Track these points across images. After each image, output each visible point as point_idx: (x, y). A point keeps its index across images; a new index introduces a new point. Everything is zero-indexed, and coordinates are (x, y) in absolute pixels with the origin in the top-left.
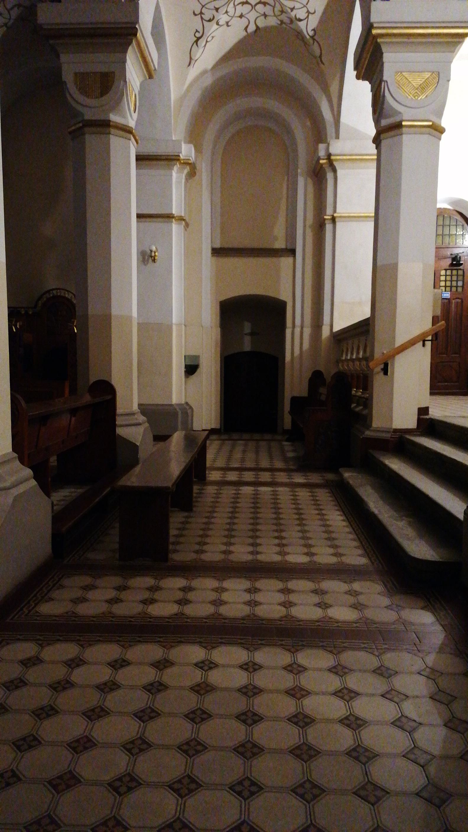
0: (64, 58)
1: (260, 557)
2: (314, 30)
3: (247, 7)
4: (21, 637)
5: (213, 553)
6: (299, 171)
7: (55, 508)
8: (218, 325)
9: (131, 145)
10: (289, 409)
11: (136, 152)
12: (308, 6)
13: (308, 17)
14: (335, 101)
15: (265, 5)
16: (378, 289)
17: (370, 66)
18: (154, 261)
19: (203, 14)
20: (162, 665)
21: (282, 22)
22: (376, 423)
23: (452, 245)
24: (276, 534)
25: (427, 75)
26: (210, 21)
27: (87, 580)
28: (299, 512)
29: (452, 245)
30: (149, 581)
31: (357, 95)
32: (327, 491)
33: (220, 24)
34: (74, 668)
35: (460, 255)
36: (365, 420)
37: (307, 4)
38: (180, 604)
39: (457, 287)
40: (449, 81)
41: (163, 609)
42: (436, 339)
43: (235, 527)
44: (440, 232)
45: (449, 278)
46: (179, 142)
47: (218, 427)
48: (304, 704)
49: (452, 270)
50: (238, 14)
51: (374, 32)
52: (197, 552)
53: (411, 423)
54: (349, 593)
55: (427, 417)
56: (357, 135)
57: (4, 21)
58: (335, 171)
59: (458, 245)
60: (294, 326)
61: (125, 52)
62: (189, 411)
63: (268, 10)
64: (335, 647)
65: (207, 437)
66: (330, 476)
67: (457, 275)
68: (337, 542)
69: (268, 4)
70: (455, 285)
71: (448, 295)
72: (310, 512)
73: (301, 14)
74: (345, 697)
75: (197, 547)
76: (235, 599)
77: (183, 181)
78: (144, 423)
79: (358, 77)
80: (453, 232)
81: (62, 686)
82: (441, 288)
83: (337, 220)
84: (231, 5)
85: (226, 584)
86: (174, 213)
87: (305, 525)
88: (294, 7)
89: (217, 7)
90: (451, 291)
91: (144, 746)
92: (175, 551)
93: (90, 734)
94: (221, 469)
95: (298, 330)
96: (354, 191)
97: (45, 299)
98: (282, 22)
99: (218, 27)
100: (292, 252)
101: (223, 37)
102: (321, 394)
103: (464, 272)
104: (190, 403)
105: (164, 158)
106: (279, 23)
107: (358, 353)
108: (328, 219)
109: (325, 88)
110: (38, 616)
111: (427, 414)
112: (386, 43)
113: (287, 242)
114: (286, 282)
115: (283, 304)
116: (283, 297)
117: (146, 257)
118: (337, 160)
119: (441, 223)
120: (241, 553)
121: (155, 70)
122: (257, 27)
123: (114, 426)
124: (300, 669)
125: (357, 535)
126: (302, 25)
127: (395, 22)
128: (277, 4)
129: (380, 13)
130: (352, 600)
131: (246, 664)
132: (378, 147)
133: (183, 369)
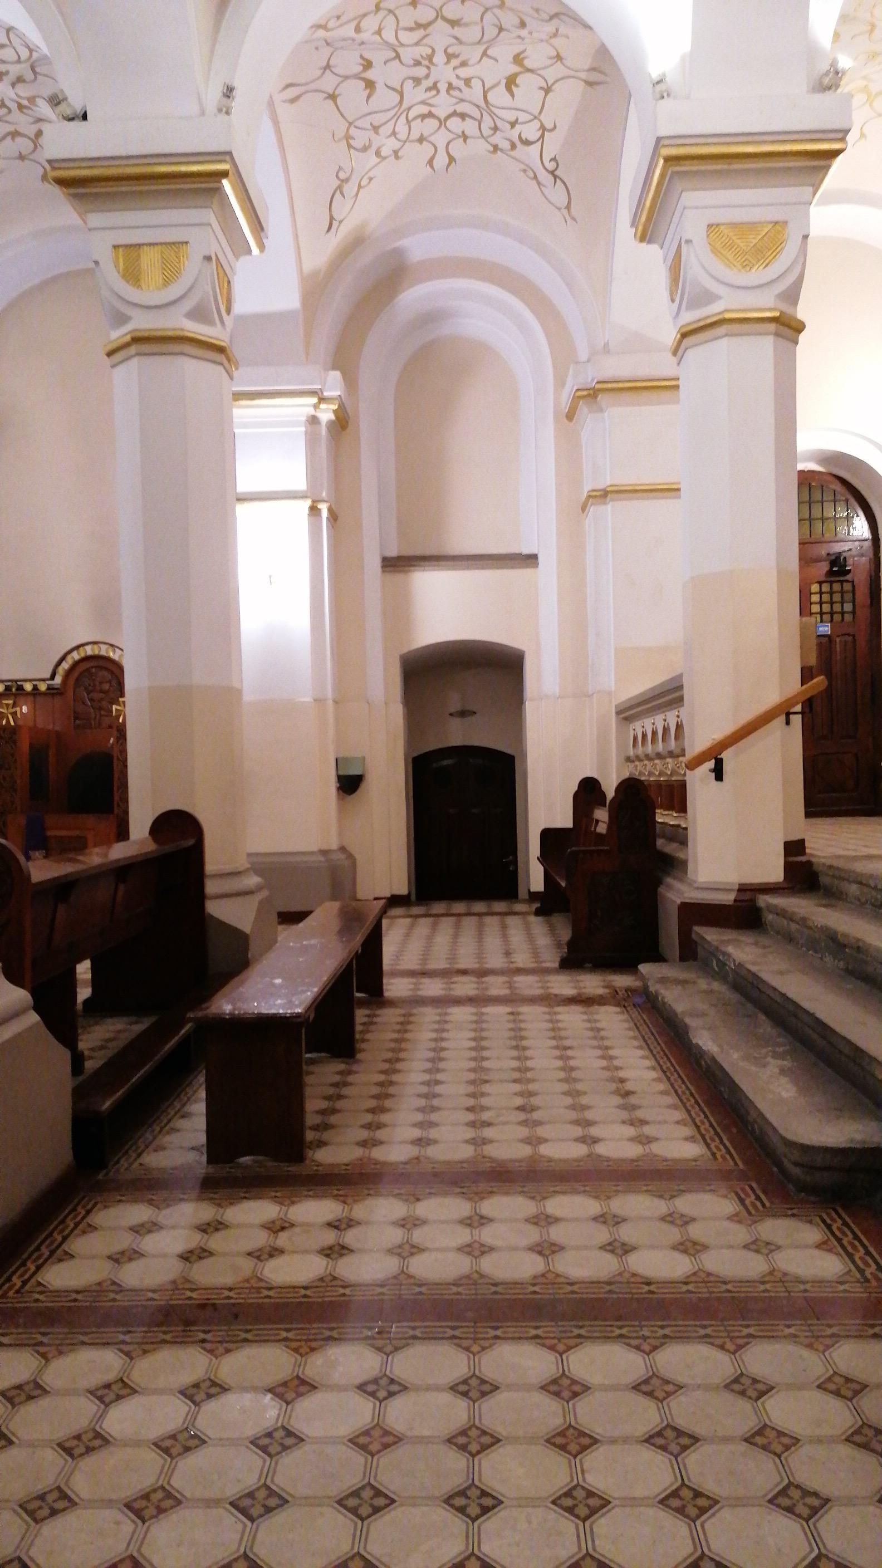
2: (554, 159)
3: (432, 124)
7: (90, 1065)
13: (542, 136)
15: (463, 119)
23: (828, 536)
26: (365, 149)
33: (383, 154)
34: (111, 1402)
35: (844, 554)
37: (540, 113)
39: (843, 613)
41: (296, 1269)
43: (438, 1089)
45: (826, 597)
49: (831, 582)
50: (415, 135)
52: (364, 1144)
55: (803, 859)
59: (840, 536)
63: (470, 127)
65: (384, 912)
66: (623, 981)
67: (842, 592)
70: (839, 609)
78: (260, 888)
80: (829, 512)
81: (84, 1444)
84: (403, 119)
87: (562, 1069)
88: (517, 119)
89: (376, 124)
90: (831, 621)
92: (321, 1144)
93: (139, 1551)
94: (412, 974)
99: (378, 160)
102: (597, 821)
103: (854, 587)
106: (492, 149)
110: (41, 1293)
123: (200, 897)
130: (674, 1234)
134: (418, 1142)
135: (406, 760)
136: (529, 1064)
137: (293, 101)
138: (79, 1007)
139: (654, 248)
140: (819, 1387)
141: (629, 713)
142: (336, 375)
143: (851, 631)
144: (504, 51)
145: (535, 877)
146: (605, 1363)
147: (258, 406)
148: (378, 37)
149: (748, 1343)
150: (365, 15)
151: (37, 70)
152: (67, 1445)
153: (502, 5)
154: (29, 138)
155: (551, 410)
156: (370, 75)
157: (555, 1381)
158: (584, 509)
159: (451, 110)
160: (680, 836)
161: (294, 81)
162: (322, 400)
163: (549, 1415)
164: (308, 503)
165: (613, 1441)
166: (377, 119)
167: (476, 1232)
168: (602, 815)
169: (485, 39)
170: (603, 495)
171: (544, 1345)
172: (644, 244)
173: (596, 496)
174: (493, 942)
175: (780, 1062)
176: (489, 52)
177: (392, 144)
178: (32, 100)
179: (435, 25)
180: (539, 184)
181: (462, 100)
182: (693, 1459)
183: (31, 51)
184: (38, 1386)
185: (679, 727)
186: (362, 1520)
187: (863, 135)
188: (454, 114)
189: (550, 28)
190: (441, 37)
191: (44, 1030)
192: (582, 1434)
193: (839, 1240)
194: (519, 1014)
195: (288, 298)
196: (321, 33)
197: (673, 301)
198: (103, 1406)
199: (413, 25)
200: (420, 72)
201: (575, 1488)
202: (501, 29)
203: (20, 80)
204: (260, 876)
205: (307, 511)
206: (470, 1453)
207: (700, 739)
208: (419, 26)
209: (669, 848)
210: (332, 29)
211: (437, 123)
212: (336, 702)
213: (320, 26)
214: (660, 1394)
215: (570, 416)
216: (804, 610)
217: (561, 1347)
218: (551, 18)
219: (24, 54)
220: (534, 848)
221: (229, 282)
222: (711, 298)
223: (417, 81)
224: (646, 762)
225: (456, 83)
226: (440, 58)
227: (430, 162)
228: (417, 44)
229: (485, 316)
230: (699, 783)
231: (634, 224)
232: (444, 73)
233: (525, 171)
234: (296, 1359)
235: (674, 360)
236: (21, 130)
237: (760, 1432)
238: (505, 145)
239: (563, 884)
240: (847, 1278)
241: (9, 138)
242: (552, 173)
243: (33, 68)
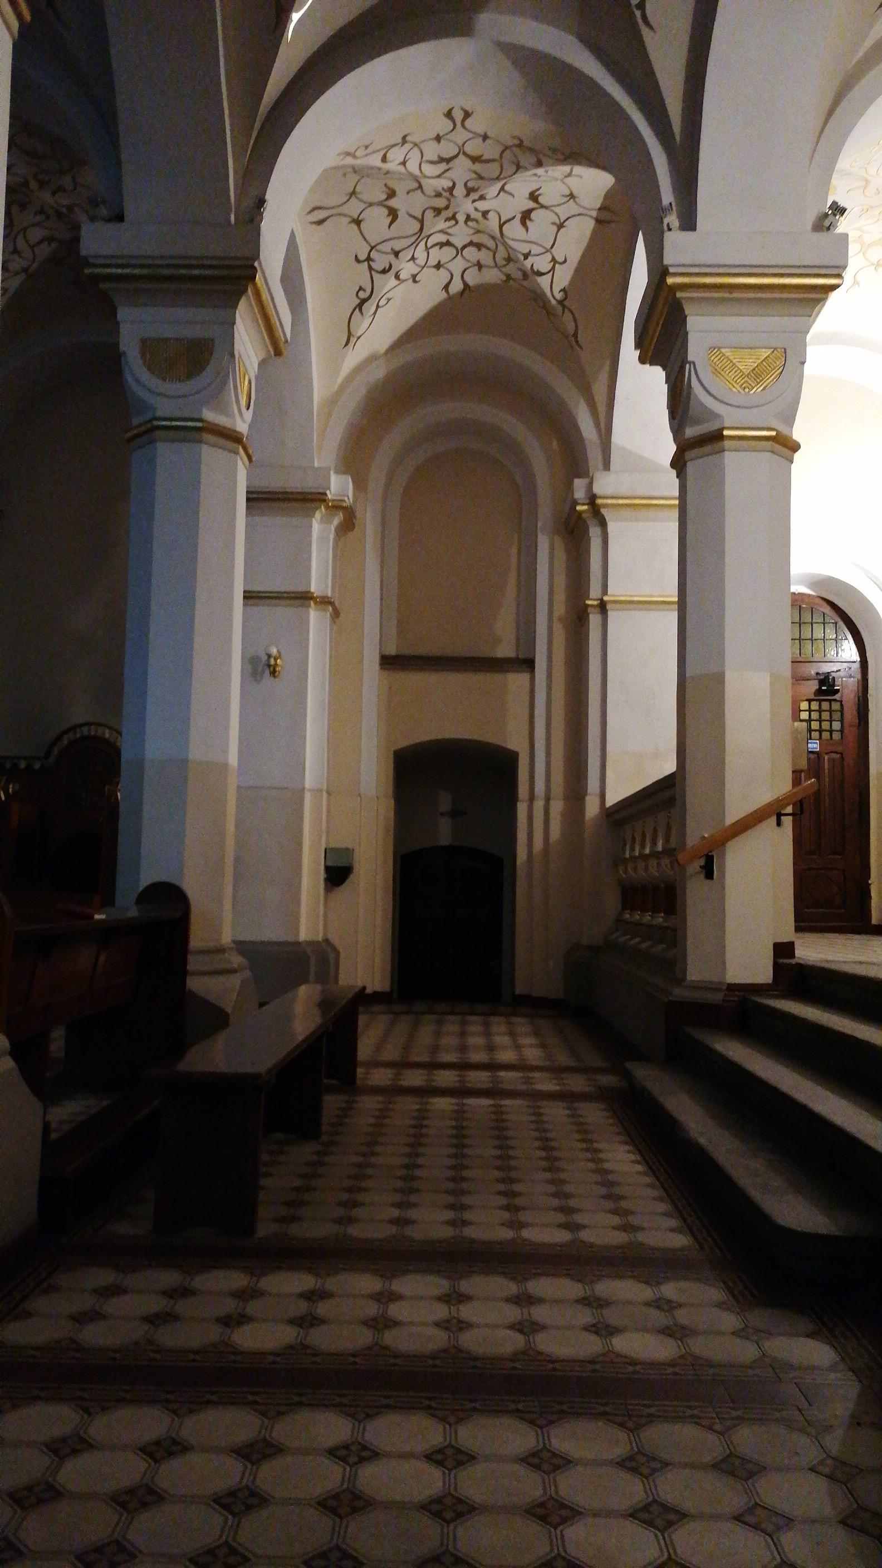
0: (124, 313)
1: (469, 1232)
2: (564, 290)
3: (448, 252)
5: (374, 1222)
6: (539, 524)
8: (391, 793)
9: (240, 462)
11: (248, 487)
13: (553, 268)
14: (602, 409)
15: (479, 250)
16: (689, 732)
17: (664, 339)
18: (274, 673)
19: (373, 260)
20: (256, 1452)
21: (509, 277)
22: (696, 971)
24: (501, 1187)
25: (765, 353)
26: (384, 271)
27: (106, 1277)
28: (546, 1144)
29: (817, 657)
30: (236, 1279)
31: (640, 391)
32: (603, 1106)
35: (833, 674)
36: (672, 966)
38: (300, 1326)
39: (831, 731)
40: (803, 363)
41: (264, 1336)
42: (802, 812)
45: (815, 715)
46: (327, 470)
47: (387, 989)
49: (820, 701)
50: (433, 262)
51: (670, 281)
53: (762, 972)
54: (657, 1304)
55: (793, 961)
56: (641, 465)
57: (25, 264)
58: (603, 523)
59: (829, 657)
60: (532, 798)
61: (235, 307)
62: (332, 956)
63: (485, 256)
64: (630, 1416)
67: (831, 711)
71: (815, 746)
73: (542, 263)
75: (340, 1212)
76: (418, 1315)
77: (332, 537)
79: (642, 360)
80: (818, 633)
83: (608, 607)
84: (422, 244)
85: (398, 1285)
86: (312, 590)
87: (558, 1170)
89: (397, 249)
95: (539, 805)
96: (640, 558)
97: (66, 742)
98: (509, 277)
99: (398, 282)
100: (528, 664)
101: (406, 301)
103: (842, 705)
104: (329, 937)
105: (301, 497)
106: (505, 278)
107: (654, 843)
108: (592, 606)
109: (586, 391)
111: (793, 956)
112: (690, 298)
113: (517, 650)
114: (520, 718)
115: (512, 758)
116: (512, 745)
117: (260, 669)
118: (607, 506)
120: (431, 1223)
121: (286, 341)
122: (466, 285)
123: (180, 971)
124: (556, 1461)
125: (666, 1190)
126: (544, 282)
128: (501, 248)
129: (680, 248)
130: (660, 1318)
131: (440, 1451)
132: (681, 474)
133: (322, 874)
134: (397, 1222)
143: (840, 749)
156: (393, 203)
159: (467, 240)
161: (322, 204)
166: (398, 245)
176: (506, 188)
178: (70, 208)
179: (457, 161)
181: (478, 232)
187: (856, 283)
188: (471, 244)
203: (61, 189)
208: (442, 160)
211: (455, 252)
213: (348, 154)
214: (645, 1471)
223: (438, 211)
225: (474, 215)
226: (459, 191)
228: (439, 176)
234: (263, 1422)
237: (750, 1510)
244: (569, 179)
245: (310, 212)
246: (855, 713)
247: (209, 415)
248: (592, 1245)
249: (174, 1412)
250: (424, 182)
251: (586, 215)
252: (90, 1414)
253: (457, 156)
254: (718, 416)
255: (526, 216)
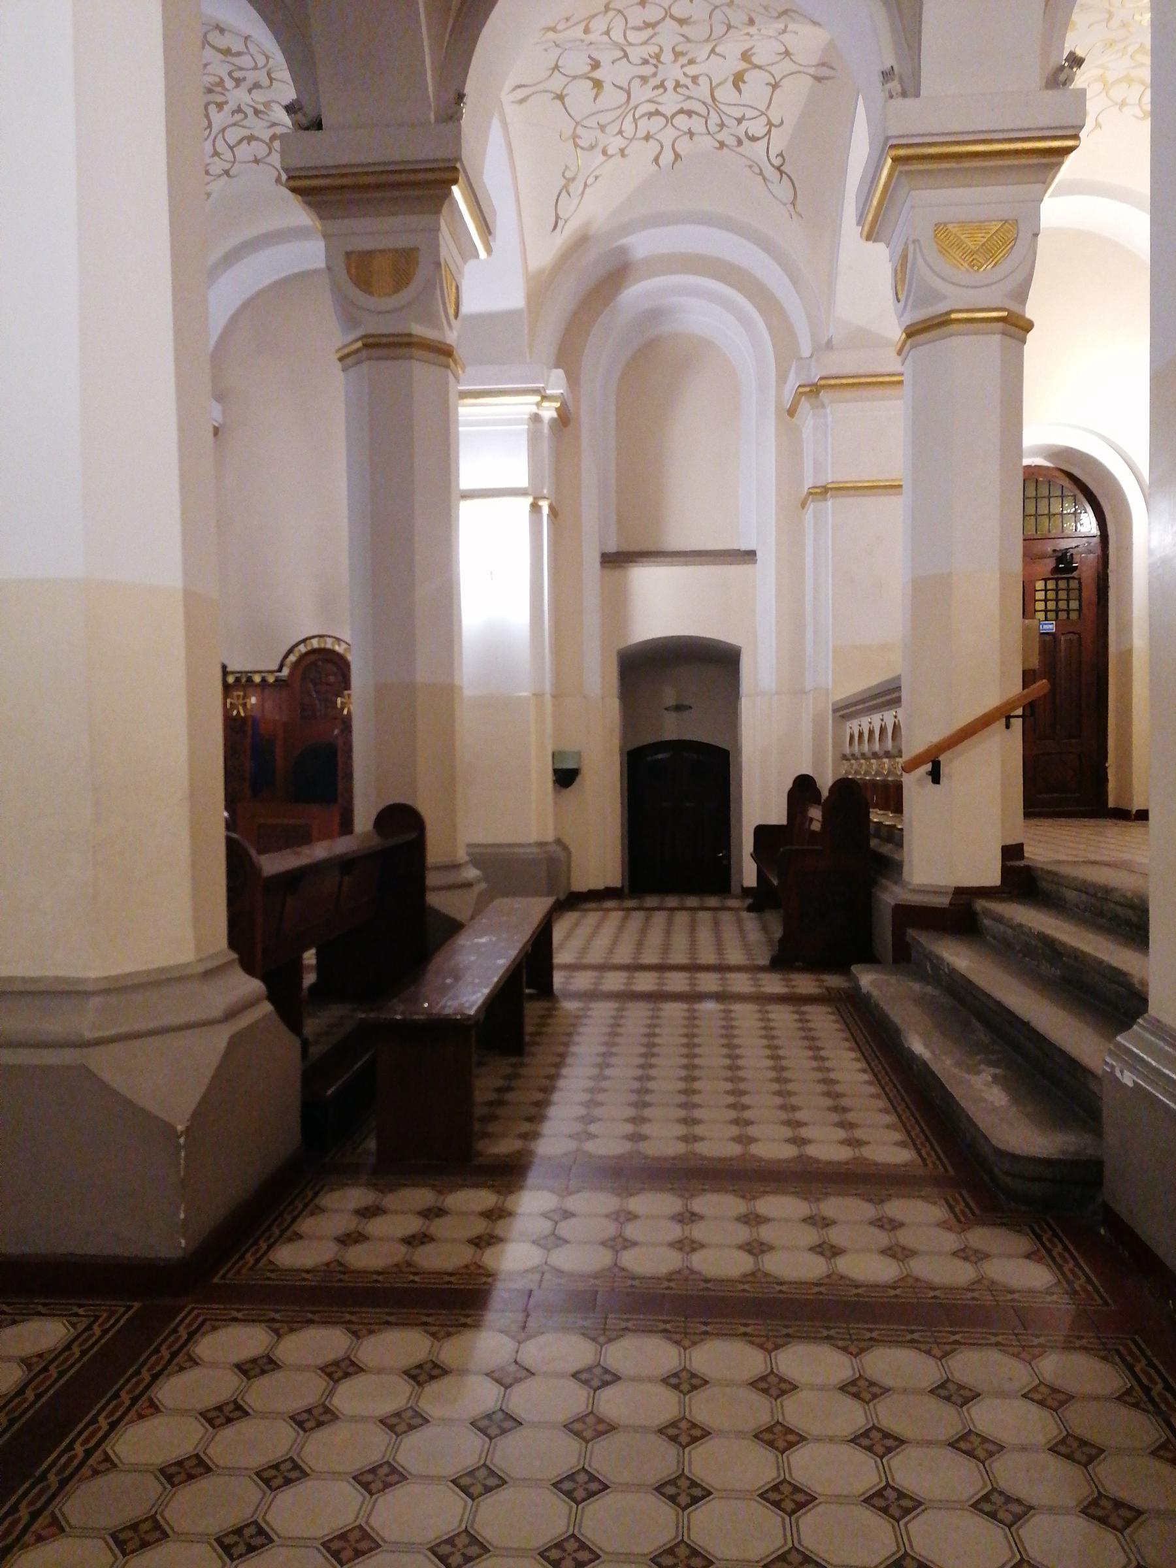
2: (781, 155)
4: (240, 1315)
7: (313, 1050)
10: (752, 850)
12: (769, 113)
13: (769, 131)
15: (690, 117)
26: (592, 147)
32: (829, 1010)
33: (609, 153)
39: (1068, 611)
40: (1036, 235)
42: (1033, 714)
44: (1031, 510)
45: (1051, 595)
48: (792, 1463)
49: (1057, 580)
50: (641, 133)
55: (1021, 863)
63: (697, 124)
66: (834, 981)
67: (1068, 590)
68: (850, 1117)
69: (696, 113)
70: (1060, 603)
72: (797, 1058)
74: (879, 1435)
80: (1056, 508)
82: (1038, 614)
84: (630, 117)
87: (774, 1068)
91: (474, 1550)
102: (811, 820)
103: (1080, 583)
106: (718, 145)
110: (272, 1271)
119: (1031, 493)
123: (421, 889)
127: (932, 135)
128: (713, 114)
135: (621, 755)
136: (740, 1062)
137: (522, 101)
138: (305, 993)
139: (881, 246)
140: (1024, 1396)
141: (845, 711)
142: (558, 374)
144: (732, 48)
145: (749, 873)
146: (813, 1364)
147: (482, 405)
148: (606, 37)
149: (955, 1350)
150: (594, 16)
151: (273, 75)
152: (298, 1418)
153: (731, 4)
154: (264, 142)
155: (773, 409)
156: (597, 74)
157: (763, 1378)
158: (803, 505)
159: (678, 107)
160: (894, 836)
162: (545, 398)
163: (758, 1411)
164: (530, 500)
165: (818, 1440)
166: (604, 118)
167: (687, 1228)
168: (815, 813)
169: (713, 37)
170: (823, 492)
171: (752, 1343)
172: (870, 243)
173: (816, 494)
174: (705, 936)
175: (992, 1070)
176: (717, 50)
177: (619, 142)
178: (267, 104)
180: (765, 179)
181: (689, 98)
182: (897, 1461)
183: (267, 58)
184: (271, 1361)
185: (896, 727)
186: (578, 1503)
187: (1098, 125)
188: (681, 111)
189: (780, 26)
190: (668, 34)
191: (276, 1019)
192: (790, 1431)
193: (1049, 1251)
194: (731, 1011)
195: (513, 298)
196: (551, 35)
197: (899, 301)
198: (332, 1383)
199: (641, 25)
200: (647, 70)
201: (781, 1483)
202: (729, 27)
203: (257, 86)
204: (479, 869)
205: (528, 508)
206: (681, 1445)
207: (916, 742)
208: (647, 25)
209: (886, 849)
210: (560, 32)
211: (664, 120)
212: (553, 696)
215: (791, 412)
216: (1028, 611)
217: (770, 1346)
218: (779, 17)
219: (261, 61)
220: (748, 844)
221: (457, 288)
222: (939, 297)
223: (644, 79)
224: (862, 761)
226: (667, 57)
227: (656, 160)
228: (645, 43)
229: (709, 315)
230: (914, 786)
231: (860, 221)
232: (672, 71)
233: (750, 167)
235: (899, 359)
236: (256, 134)
237: (964, 1437)
238: (731, 141)
239: (775, 883)
240: (1056, 1290)
241: (245, 142)
242: (778, 169)
243: (269, 74)
244: (785, 35)
245: (514, 90)
246: (1095, 590)
247: (419, 330)
248: (817, 1161)
249: (434, 1335)
250: (628, 49)
251: (800, 72)
252: (358, 1338)
253: (663, 19)
254: (942, 297)
255: (738, 80)
